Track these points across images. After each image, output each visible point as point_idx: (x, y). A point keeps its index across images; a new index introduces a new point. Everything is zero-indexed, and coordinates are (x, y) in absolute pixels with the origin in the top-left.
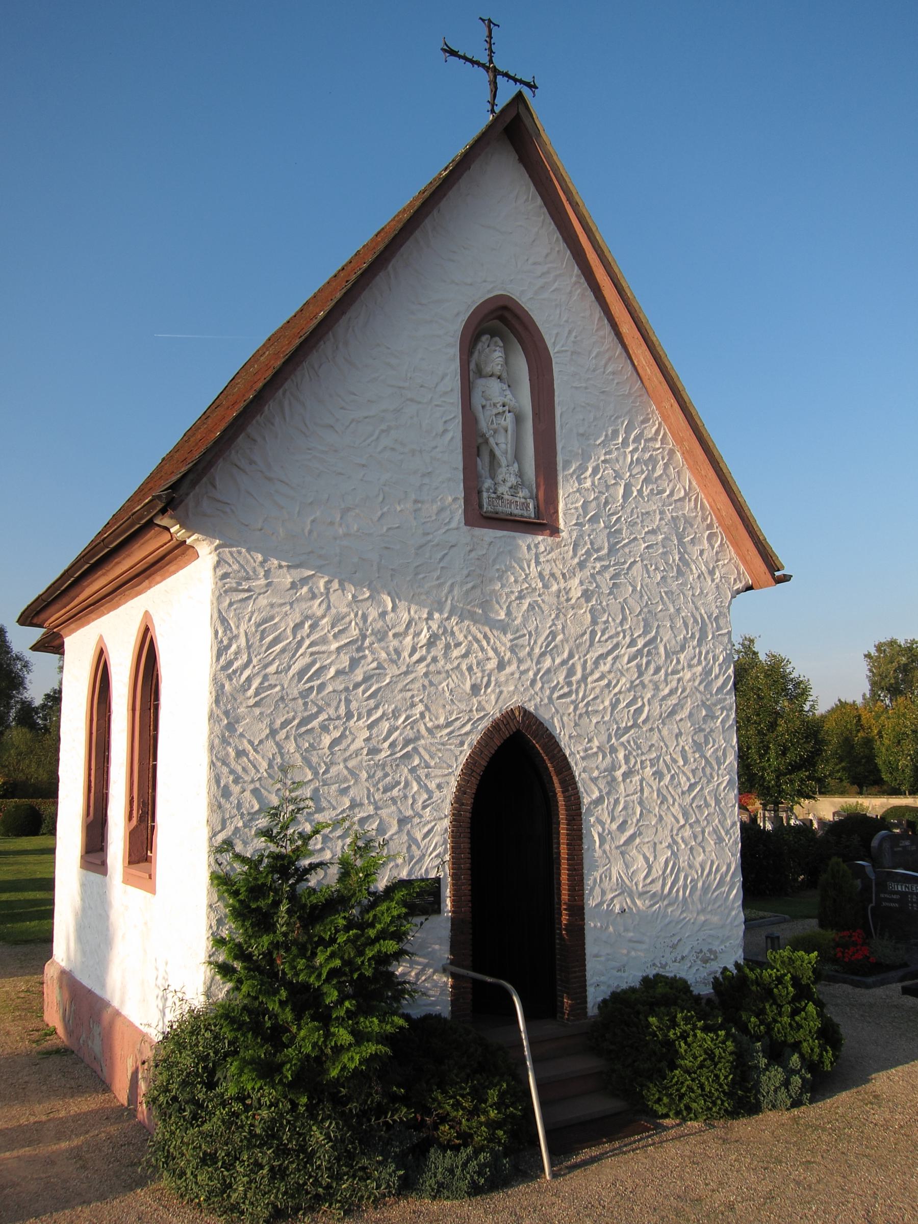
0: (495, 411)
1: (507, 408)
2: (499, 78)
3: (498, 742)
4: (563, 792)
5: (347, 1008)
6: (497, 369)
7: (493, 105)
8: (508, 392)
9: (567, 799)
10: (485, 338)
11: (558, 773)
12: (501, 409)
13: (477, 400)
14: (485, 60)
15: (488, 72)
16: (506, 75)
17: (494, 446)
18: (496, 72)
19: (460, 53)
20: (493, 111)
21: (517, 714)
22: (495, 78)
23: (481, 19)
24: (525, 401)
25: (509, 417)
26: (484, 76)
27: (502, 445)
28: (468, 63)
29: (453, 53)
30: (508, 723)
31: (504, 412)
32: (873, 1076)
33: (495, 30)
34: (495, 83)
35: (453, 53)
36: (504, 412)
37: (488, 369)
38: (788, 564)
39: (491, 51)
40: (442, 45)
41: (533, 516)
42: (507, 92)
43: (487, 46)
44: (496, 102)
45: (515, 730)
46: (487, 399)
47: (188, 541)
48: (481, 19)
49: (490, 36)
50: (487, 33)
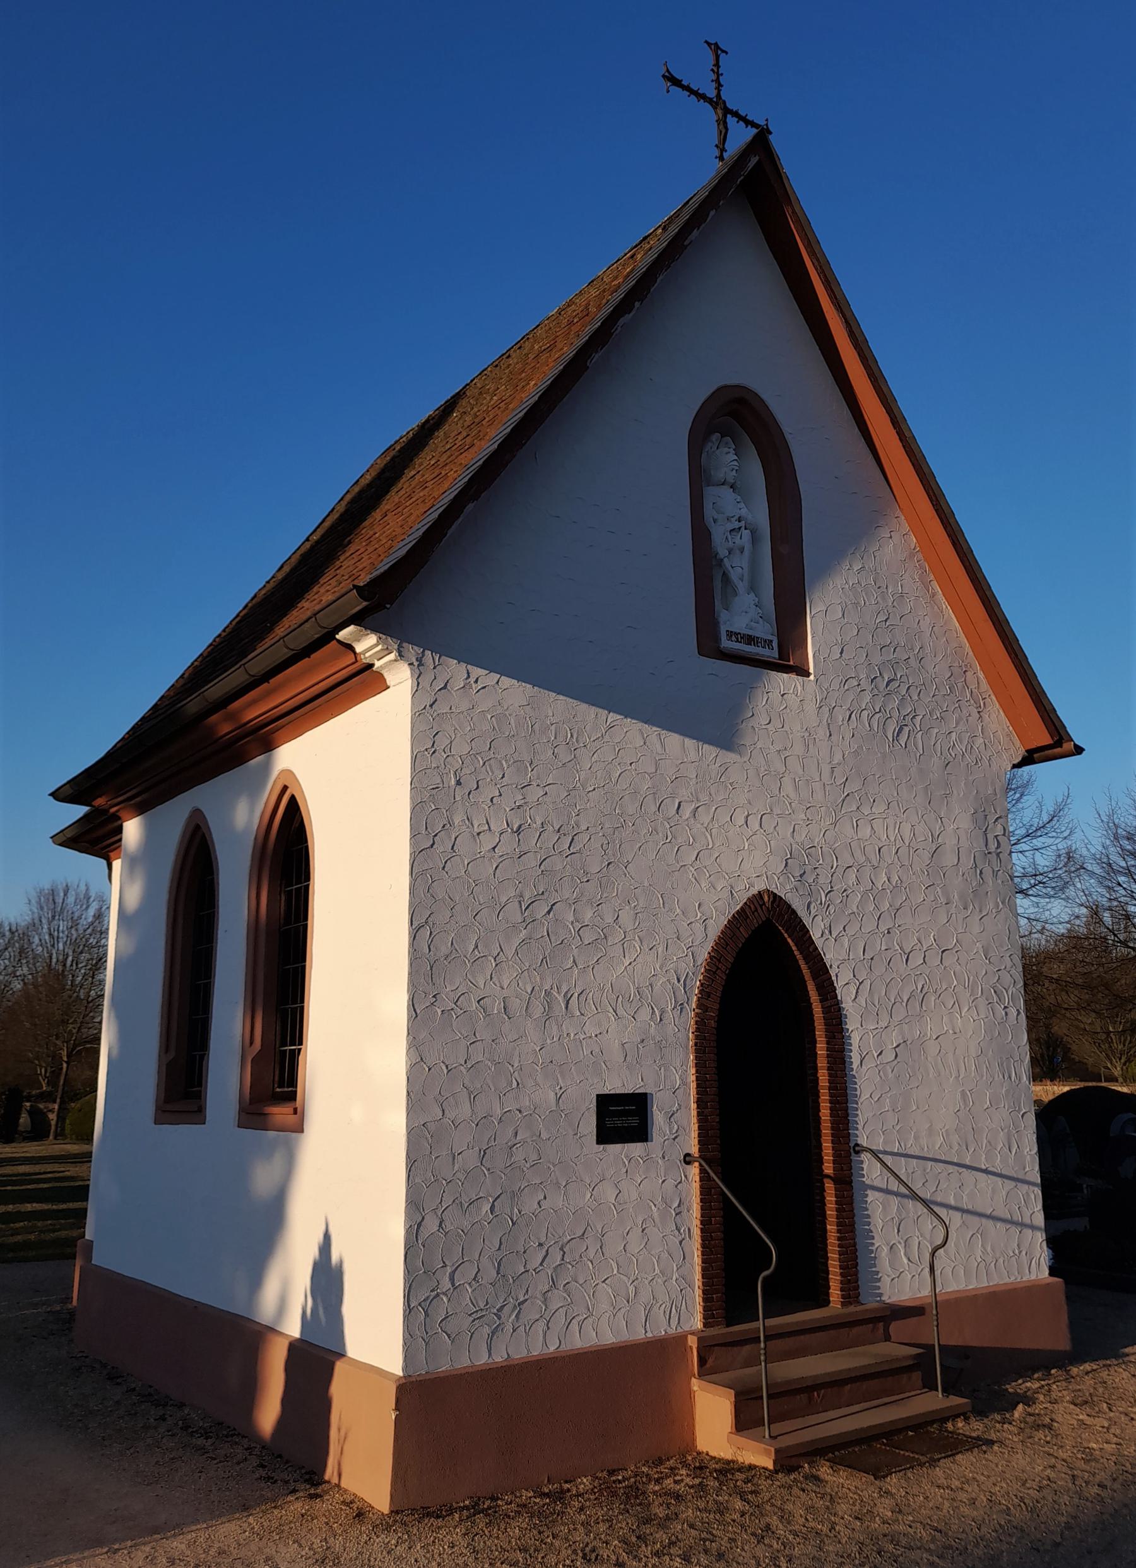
0: (730, 526)
1: (743, 524)
2: (729, 116)
3: (744, 933)
4: (821, 1001)
5: (55, 1102)
6: (731, 476)
7: (723, 150)
8: (742, 505)
9: (826, 1011)
10: (716, 436)
11: (815, 977)
12: (736, 525)
13: (709, 512)
14: (711, 93)
15: (715, 108)
16: (736, 114)
17: (730, 568)
18: (727, 111)
19: (685, 83)
20: (721, 158)
21: (766, 898)
22: (725, 116)
23: (706, 42)
24: (760, 514)
25: (746, 533)
26: (710, 115)
27: (737, 568)
28: (693, 96)
29: (676, 82)
30: (756, 910)
31: (740, 528)
32: (1127, 1350)
33: (722, 56)
34: (725, 123)
35: (676, 82)
36: (740, 528)
37: (720, 475)
38: (1077, 734)
39: (717, 81)
40: (663, 71)
41: (777, 656)
42: (740, 137)
43: (714, 77)
44: (726, 146)
45: (764, 919)
46: (718, 512)
47: (378, 664)
48: (706, 42)
49: (717, 65)
50: (712, 62)
